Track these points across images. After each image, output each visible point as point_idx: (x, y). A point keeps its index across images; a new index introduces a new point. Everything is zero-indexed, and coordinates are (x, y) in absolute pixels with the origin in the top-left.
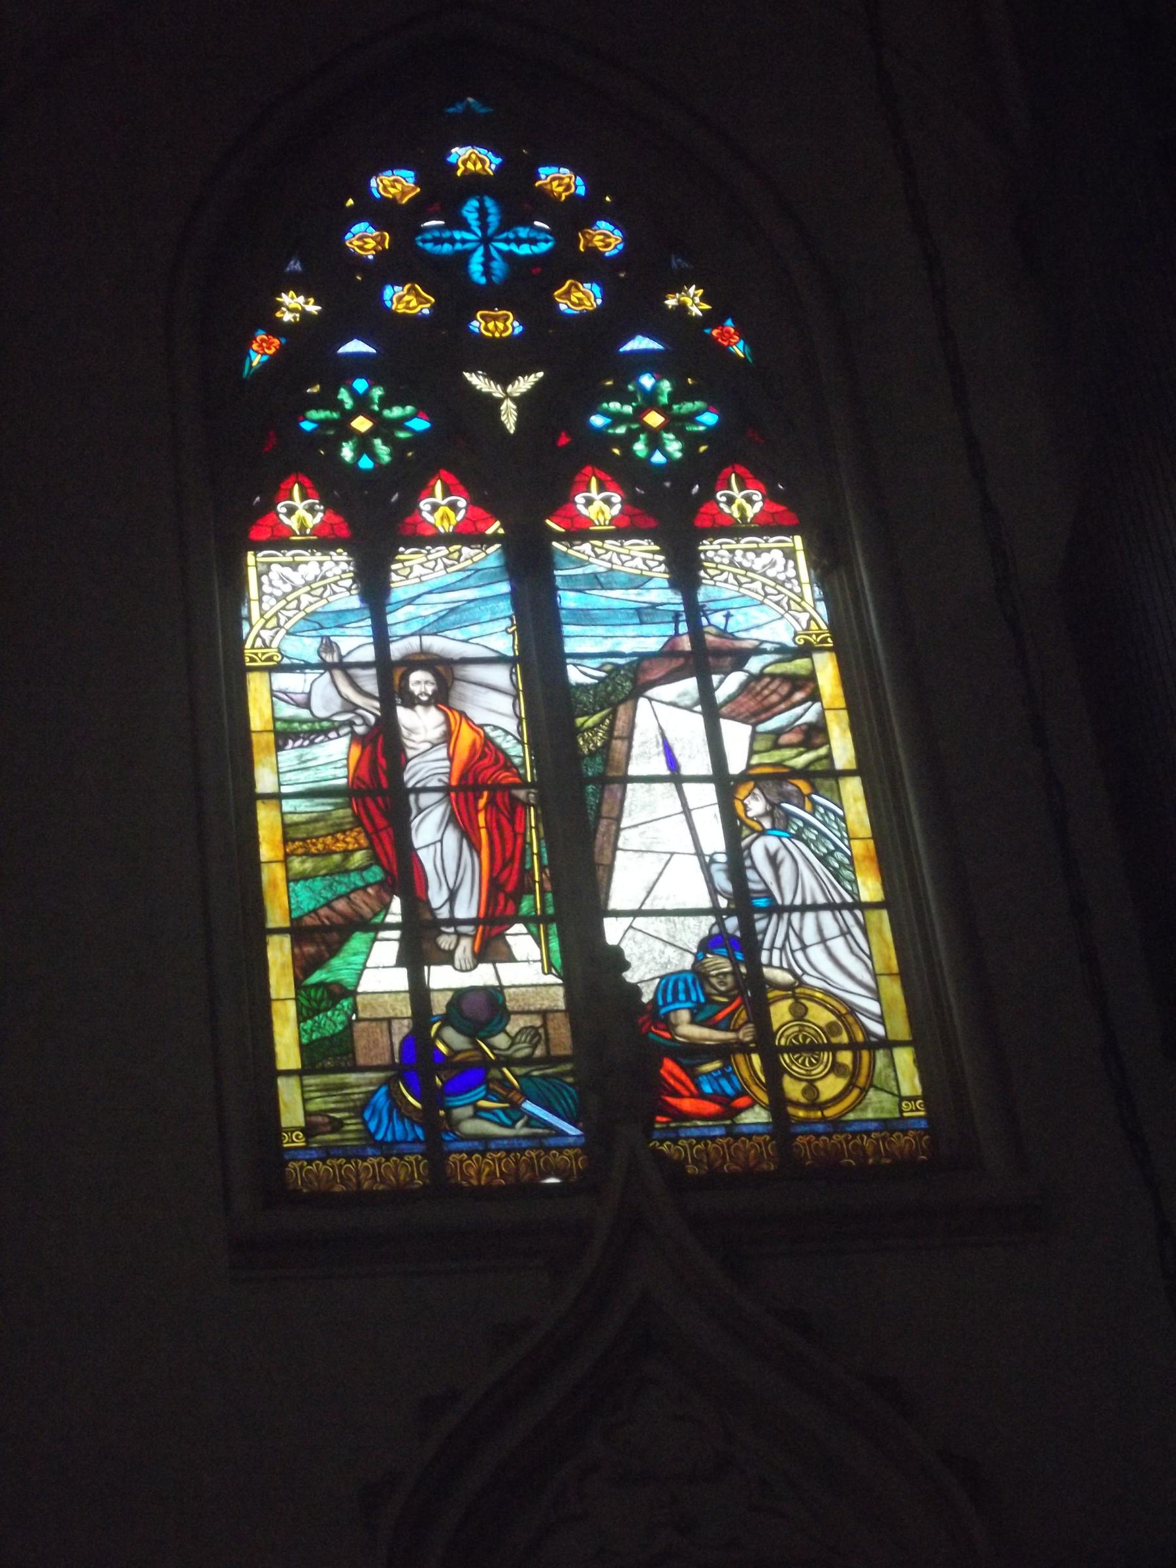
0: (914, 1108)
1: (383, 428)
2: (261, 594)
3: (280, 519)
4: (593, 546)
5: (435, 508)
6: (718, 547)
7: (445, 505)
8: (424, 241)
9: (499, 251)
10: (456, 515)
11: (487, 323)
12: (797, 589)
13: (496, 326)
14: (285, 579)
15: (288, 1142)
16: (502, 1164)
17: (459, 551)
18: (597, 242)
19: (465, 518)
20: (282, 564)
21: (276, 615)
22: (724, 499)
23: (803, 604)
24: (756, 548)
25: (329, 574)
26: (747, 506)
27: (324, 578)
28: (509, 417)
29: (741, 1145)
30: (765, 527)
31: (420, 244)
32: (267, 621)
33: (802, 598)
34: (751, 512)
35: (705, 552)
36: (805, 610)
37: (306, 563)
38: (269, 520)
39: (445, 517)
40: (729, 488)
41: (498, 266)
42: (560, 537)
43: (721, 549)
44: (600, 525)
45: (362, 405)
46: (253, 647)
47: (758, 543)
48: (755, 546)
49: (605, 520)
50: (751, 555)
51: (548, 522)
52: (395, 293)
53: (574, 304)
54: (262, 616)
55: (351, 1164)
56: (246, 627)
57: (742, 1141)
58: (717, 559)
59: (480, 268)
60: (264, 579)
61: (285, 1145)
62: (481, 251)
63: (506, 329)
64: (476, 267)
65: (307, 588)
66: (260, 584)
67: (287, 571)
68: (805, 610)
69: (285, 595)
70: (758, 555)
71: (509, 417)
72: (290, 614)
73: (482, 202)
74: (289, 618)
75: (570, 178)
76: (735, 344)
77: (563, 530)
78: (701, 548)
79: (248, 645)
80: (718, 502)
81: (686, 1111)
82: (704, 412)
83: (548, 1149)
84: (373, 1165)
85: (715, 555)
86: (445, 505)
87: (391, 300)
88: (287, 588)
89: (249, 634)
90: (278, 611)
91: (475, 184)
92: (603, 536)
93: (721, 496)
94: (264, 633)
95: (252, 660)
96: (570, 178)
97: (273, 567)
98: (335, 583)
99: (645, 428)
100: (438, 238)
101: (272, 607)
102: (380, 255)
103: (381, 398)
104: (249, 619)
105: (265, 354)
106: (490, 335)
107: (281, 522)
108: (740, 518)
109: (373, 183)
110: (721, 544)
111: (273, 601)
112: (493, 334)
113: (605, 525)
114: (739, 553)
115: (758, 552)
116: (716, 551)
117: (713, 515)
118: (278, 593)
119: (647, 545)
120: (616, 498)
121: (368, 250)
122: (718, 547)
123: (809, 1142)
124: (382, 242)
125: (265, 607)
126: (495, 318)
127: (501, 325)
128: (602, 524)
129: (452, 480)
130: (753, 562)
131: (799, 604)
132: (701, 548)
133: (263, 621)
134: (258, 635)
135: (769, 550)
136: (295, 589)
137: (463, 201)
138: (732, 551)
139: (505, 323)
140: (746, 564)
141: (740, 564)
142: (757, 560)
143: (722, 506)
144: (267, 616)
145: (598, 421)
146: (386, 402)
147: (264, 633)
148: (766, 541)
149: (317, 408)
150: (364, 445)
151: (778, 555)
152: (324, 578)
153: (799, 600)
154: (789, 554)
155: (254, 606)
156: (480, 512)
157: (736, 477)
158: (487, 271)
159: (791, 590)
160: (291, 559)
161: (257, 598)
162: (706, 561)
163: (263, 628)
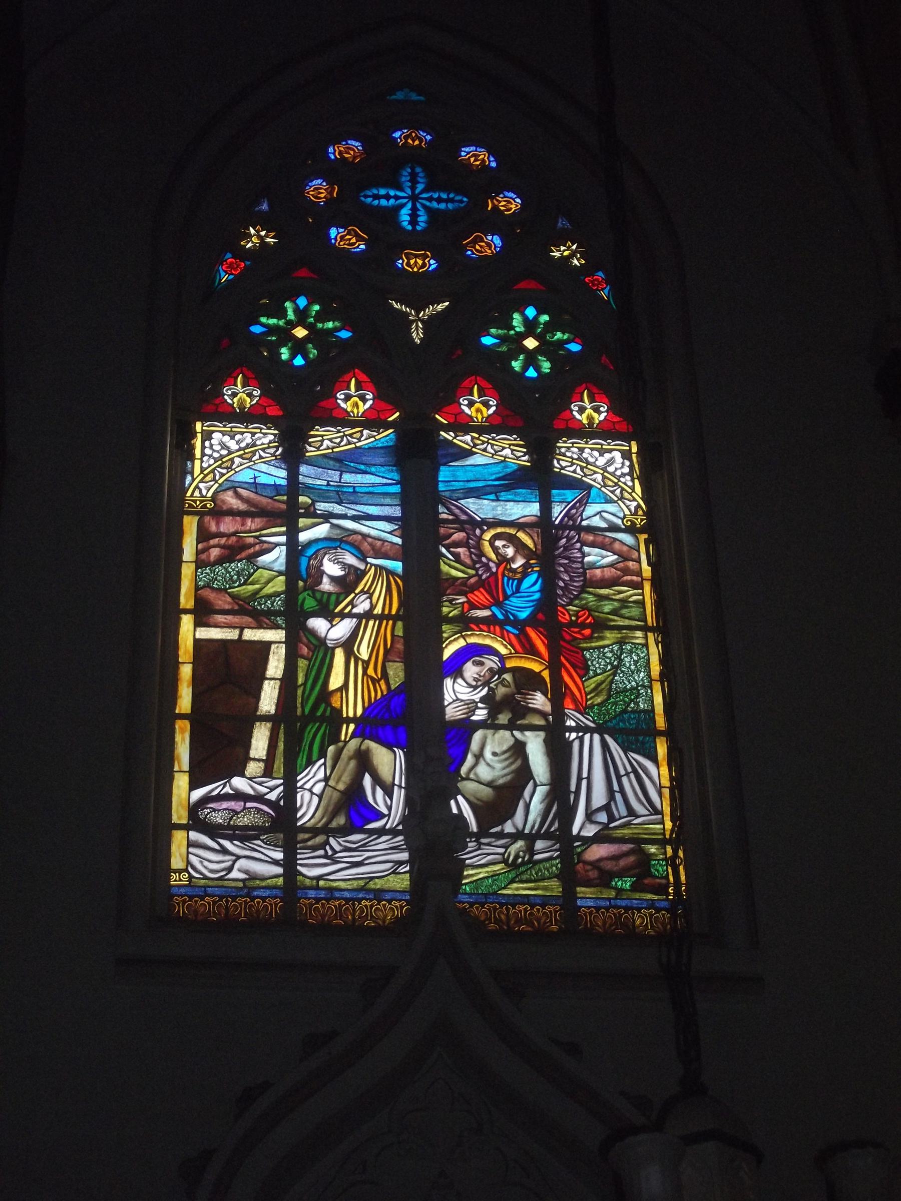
0: (177, 879)
1: (315, 335)
2: (203, 454)
3: (462, 409)
4: (473, 438)
5: (471, 404)
6: (571, 445)
7: (479, 402)
8: (366, 196)
9: (424, 206)
10: (364, 405)
11: (409, 259)
12: (630, 484)
13: (416, 262)
14: (223, 446)
15: (175, 880)
16: (185, 906)
17: (361, 432)
18: (502, 206)
19: (371, 407)
20: (224, 434)
21: (213, 471)
22: (576, 408)
23: (633, 494)
24: (600, 448)
25: (258, 443)
26: (595, 415)
27: (254, 445)
28: (417, 335)
29: (193, 904)
30: (605, 432)
31: (363, 199)
32: (206, 476)
33: (633, 490)
34: (363, 407)
35: (560, 448)
36: (634, 500)
37: (242, 433)
38: (564, 416)
39: (356, 405)
40: (582, 401)
41: (423, 218)
42: (447, 429)
43: (573, 447)
44: (354, 417)
45: (302, 317)
46: (192, 495)
47: (602, 445)
48: (600, 446)
49: (358, 413)
50: (596, 454)
51: (437, 416)
52: (339, 233)
53: (477, 250)
54: (202, 472)
55: (380, 906)
56: (189, 478)
57: (662, 914)
58: (568, 454)
59: (408, 218)
60: (207, 444)
61: (172, 883)
62: (409, 205)
63: (424, 265)
64: (404, 216)
65: (242, 452)
66: (203, 447)
67: (226, 439)
68: (634, 500)
69: (222, 457)
70: (601, 455)
71: (417, 335)
72: (224, 471)
73: (413, 169)
74: (223, 475)
75: (485, 155)
76: (603, 289)
77: (446, 422)
78: (558, 445)
79: (189, 494)
80: (572, 411)
81: (260, 874)
82: (570, 343)
83: (253, 899)
84: (551, 912)
85: (567, 451)
86: (479, 402)
87: (336, 239)
88: (224, 452)
89: (190, 485)
90: (215, 469)
91: (410, 156)
92: (353, 424)
93: (227, 391)
94: (201, 485)
95: (190, 506)
96: (485, 155)
97: (215, 435)
98: (263, 450)
99: (525, 350)
100: (376, 194)
101: (210, 466)
102: (329, 201)
103: (317, 312)
104: (192, 473)
105: (232, 274)
106: (410, 269)
107: (574, 417)
108: (588, 424)
109: (331, 150)
110: (573, 443)
111: (212, 461)
112: (412, 269)
113: (357, 417)
114: (587, 451)
115: (602, 452)
116: (568, 448)
117: (567, 421)
118: (216, 455)
119: (512, 439)
120: (493, 402)
121: (320, 198)
122: (571, 445)
123: (372, 906)
124: (331, 193)
125: (205, 465)
126: (416, 256)
127: (420, 262)
128: (356, 416)
129: (363, 377)
130: (597, 460)
131: (630, 494)
132: (558, 445)
133: (202, 476)
134: (197, 487)
135: (610, 451)
136: (230, 453)
137: (402, 166)
138: (582, 450)
139: (424, 261)
140: (591, 460)
141: (586, 459)
142: (600, 459)
143: (575, 413)
144: (205, 472)
145: (256, 329)
146: (322, 317)
147: (201, 485)
148: (609, 444)
149: (269, 316)
150: (531, 358)
151: (617, 455)
152: (254, 445)
153: (630, 491)
154: (626, 455)
155: (197, 463)
156: (383, 405)
157: (478, 388)
158: (413, 221)
159: (625, 484)
160: (229, 429)
161: (199, 457)
162: (559, 454)
163: (201, 481)
